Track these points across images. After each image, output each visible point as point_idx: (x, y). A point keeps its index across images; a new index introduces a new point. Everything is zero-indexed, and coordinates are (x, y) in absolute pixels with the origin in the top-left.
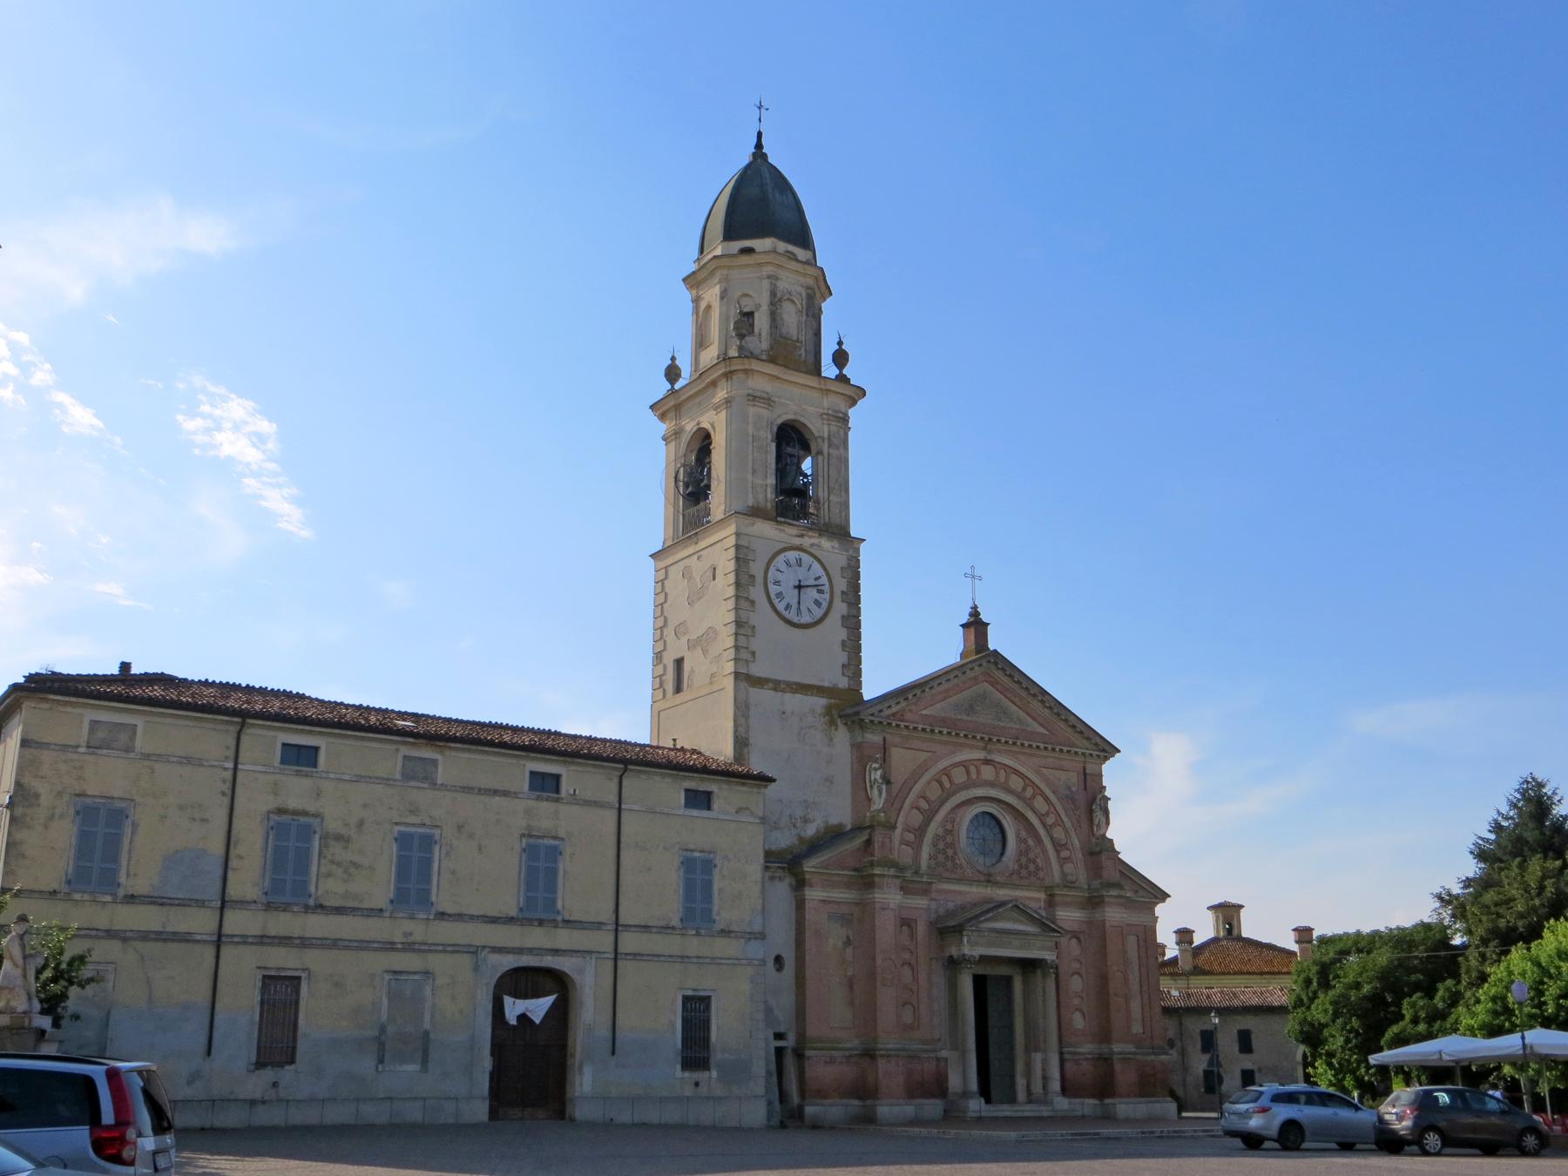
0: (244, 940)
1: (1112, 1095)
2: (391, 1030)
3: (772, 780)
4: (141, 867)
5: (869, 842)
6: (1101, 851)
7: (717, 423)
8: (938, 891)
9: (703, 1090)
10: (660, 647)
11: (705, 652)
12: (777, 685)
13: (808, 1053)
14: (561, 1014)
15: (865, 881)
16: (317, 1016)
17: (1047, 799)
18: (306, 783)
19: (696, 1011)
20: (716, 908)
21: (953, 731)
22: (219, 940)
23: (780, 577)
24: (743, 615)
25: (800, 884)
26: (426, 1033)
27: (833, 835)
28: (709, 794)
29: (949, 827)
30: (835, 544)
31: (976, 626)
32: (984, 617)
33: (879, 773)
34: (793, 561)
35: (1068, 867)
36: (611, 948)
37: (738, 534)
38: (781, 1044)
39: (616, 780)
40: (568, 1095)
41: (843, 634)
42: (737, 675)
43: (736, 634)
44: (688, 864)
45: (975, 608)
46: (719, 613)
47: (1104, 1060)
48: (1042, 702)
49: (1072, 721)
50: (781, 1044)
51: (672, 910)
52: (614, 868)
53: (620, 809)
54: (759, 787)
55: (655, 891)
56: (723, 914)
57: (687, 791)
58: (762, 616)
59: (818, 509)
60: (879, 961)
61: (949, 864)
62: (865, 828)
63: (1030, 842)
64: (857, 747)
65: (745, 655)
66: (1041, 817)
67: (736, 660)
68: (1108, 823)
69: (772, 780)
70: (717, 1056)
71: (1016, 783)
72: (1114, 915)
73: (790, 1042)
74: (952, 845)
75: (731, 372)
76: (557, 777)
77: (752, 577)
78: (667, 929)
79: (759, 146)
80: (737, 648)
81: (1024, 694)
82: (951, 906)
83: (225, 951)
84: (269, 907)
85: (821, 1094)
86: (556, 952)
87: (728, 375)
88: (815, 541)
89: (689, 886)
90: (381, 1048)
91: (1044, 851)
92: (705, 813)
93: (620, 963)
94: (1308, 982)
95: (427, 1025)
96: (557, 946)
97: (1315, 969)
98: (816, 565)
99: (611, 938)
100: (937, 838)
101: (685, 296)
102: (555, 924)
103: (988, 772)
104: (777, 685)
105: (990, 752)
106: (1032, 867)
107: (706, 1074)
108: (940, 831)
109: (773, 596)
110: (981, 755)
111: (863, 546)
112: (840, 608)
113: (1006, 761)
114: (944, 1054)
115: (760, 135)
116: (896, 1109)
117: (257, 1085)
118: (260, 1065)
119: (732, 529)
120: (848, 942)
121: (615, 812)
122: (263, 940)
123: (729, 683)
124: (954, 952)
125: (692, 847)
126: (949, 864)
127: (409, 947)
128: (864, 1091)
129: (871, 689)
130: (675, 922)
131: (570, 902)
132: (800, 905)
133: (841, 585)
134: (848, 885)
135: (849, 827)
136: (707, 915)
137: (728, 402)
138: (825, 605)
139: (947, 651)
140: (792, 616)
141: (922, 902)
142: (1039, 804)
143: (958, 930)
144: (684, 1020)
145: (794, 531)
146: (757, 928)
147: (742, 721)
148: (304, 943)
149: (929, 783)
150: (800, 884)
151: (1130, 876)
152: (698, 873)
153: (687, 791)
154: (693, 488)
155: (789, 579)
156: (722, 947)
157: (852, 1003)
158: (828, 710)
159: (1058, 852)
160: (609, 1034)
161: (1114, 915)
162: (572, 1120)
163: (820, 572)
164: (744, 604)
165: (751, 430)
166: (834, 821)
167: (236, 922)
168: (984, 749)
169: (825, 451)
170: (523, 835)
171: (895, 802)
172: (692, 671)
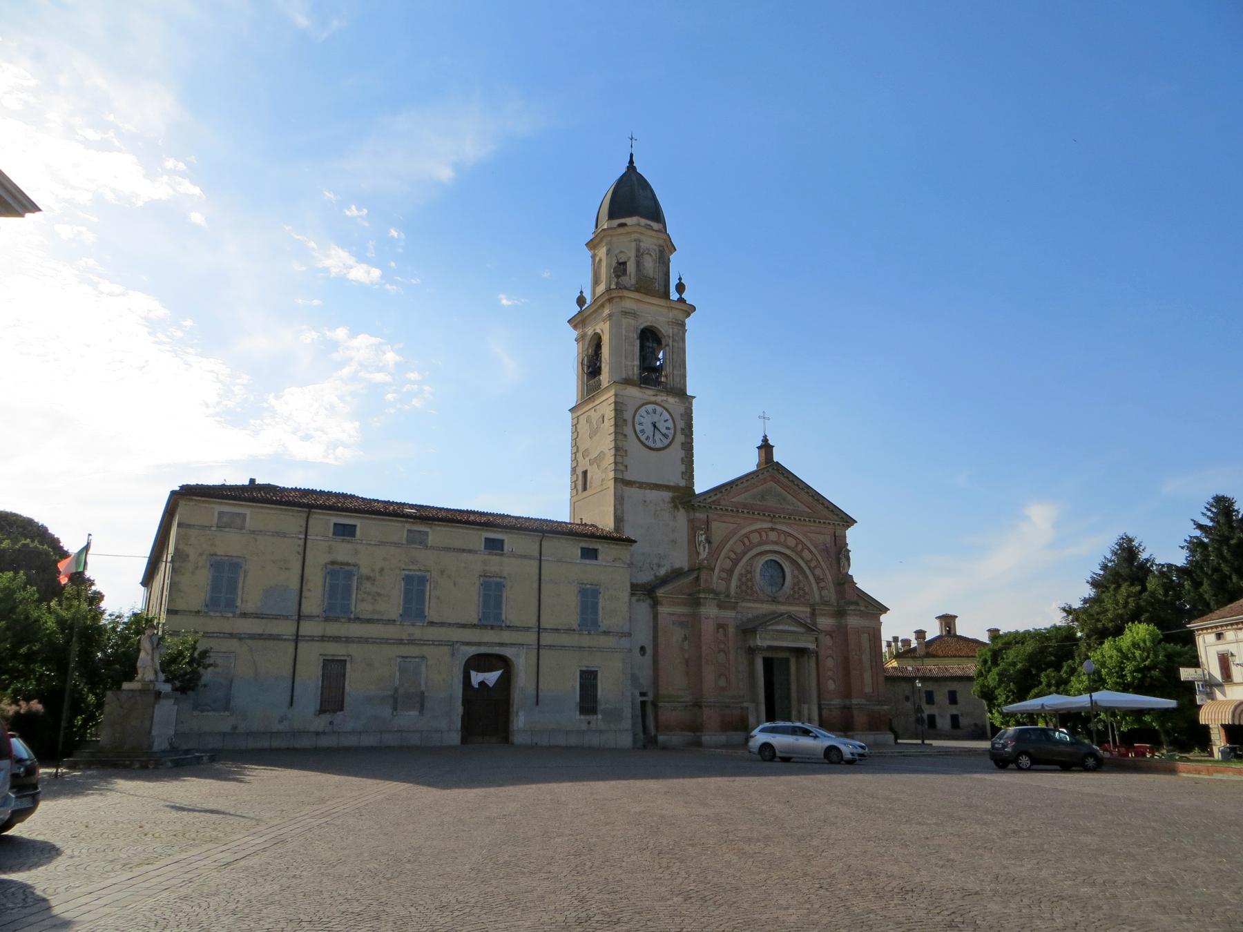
0: (312, 639)
2: (401, 691)
3: (635, 542)
4: (250, 596)
6: (845, 582)
7: (603, 328)
12: (641, 485)
15: (695, 602)
16: (356, 684)
17: (811, 552)
18: (349, 546)
19: (589, 680)
21: (752, 511)
22: (297, 639)
23: (642, 420)
25: (655, 603)
26: (423, 693)
27: (677, 574)
31: (766, 448)
32: (771, 442)
35: (824, 593)
37: (616, 395)
38: (644, 699)
41: (682, 454)
42: (616, 479)
45: (765, 437)
47: (847, 709)
50: (644, 699)
51: (573, 620)
55: (563, 608)
56: (605, 622)
58: (632, 445)
60: (704, 648)
62: (696, 570)
63: (801, 577)
65: (621, 467)
70: (601, 706)
72: (853, 621)
73: (649, 698)
74: (751, 580)
76: (502, 541)
77: (625, 421)
78: (570, 631)
79: (631, 162)
80: (616, 463)
83: (300, 645)
84: (327, 619)
87: (610, 300)
90: (396, 701)
92: (594, 562)
94: (985, 662)
95: (423, 688)
98: (665, 413)
99: (535, 636)
102: (501, 628)
103: (773, 536)
110: (769, 525)
113: (784, 528)
115: (631, 155)
117: (320, 723)
118: (322, 711)
119: (612, 392)
120: (685, 638)
121: (536, 563)
122: (323, 638)
123: (611, 484)
124: (752, 644)
127: (412, 642)
128: (696, 727)
129: (700, 487)
130: (575, 627)
132: (655, 617)
133: (681, 424)
136: (595, 623)
137: (610, 316)
139: (749, 462)
141: (731, 614)
142: (806, 554)
145: (651, 392)
146: (626, 629)
148: (348, 640)
154: (592, 368)
156: (604, 641)
158: (673, 500)
161: (853, 621)
166: (677, 566)
167: (308, 628)
171: (714, 554)
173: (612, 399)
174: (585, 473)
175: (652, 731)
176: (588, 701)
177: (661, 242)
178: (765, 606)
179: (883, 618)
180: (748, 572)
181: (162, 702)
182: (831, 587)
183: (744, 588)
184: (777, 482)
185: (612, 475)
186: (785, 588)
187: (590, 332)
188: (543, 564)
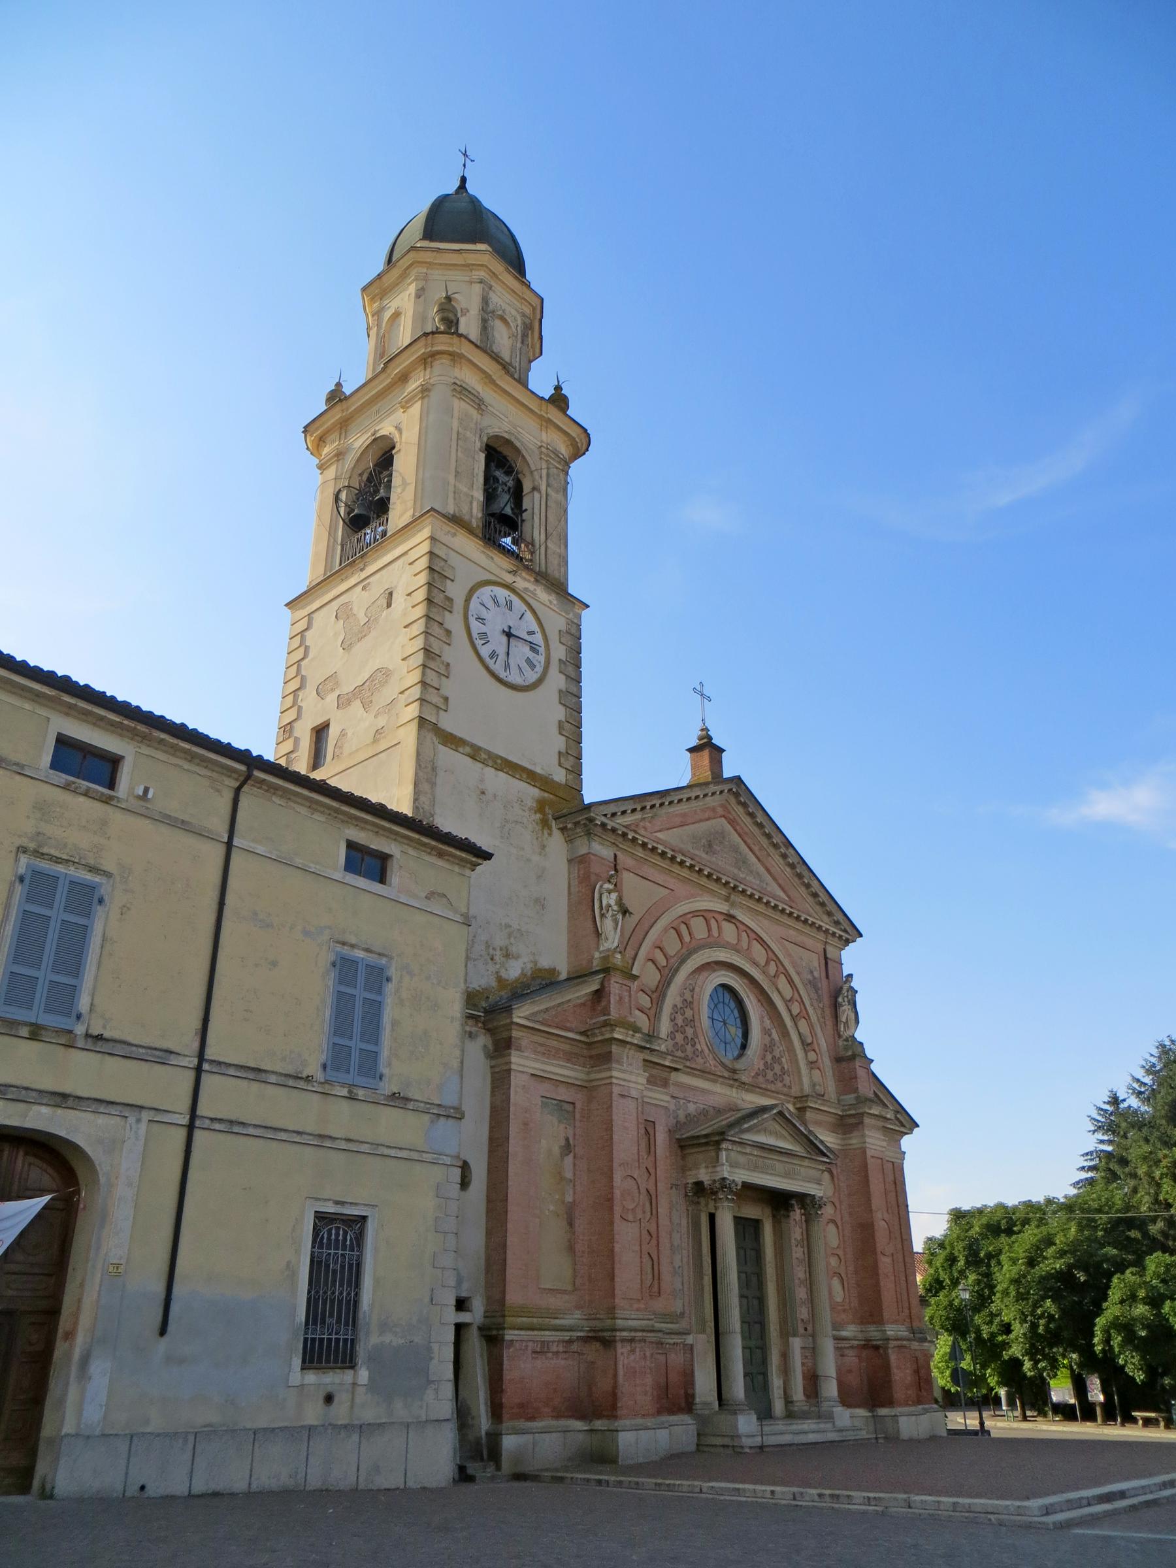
1: (890, 1403)
3: (487, 856)
5: (599, 994)
6: (850, 1058)
7: (404, 425)
8: (679, 1085)
9: (340, 1412)
10: (291, 715)
11: (366, 706)
12: (476, 753)
13: (509, 1335)
14: (53, 1243)
15: (596, 1052)
17: (791, 981)
19: (338, 1243)
20: (385, 1053)
23: (484, 613)
24: (436, 647)
25: (501, 1046)
27: (543, 982)
28: (384, 858)
29: (688, 996)
30: (553, 598)
31: (707, 748)
33: (614, 896)
34: (502, 601)
36: (184, 1105)
37: (433, 539)
38: (465, 1317)
39: (228, 796)
40: (47, 1431)
41: (560, 713)
42: (422, 721)
43: (424, 666)
44: (345, 968)
45: (706, 729)
46: (396, 648)
48: (784, 856)
49: (815, 887)
50: (465, 1317)
52: (212, 918)
53: (229, 845)
54: (462, 862)
55: (279, 1010)
56: (397, 1070)
57: (351, 845)
58: (458, 654)
59: (532, 553)
61: (689, 1047)
62: (597, 977)
63: (775, 1035)
64: (579, 862)
65: (434, 698)
66: (788, 1002)
67: (422, 700)
68: (857, 1022)
69: (487, 856)
70: (370, 1340)
71: (758, 952)
72: (874, 1141)
73: (475, 1315)
74: (691, 1022)
75: (433, 355)
76: (114, 761)
77: (450, 600)
78: (295, 1080)
80: (424, 683)
81: (764, 842)
82: (692, 1108)
85: (528, 1412)
86: (62, 1099)
87: (427, 360)
88: (531, 587)
89: (343, 1007)
91: (791, 1049)
92: (376, 887)
93: (198, 1135)
94: (952, 1260)
96: (67, 1088)
97: (959, 1246)
98: (529, 615)
100: (676, 1010)
101: (283, 623)
104: (476, 753)
105: (733, 905)
106: (777, 1068)
107: (348, 1376)
108: (678, 1001)
109: (475, 635)
110: (723, 907)
111: (586, 615)
112: (556, 680)
114: (690, 1339)
116: (645, 1435)
119: (426, 532)
120: (567, 1148)
121: (221, 850)
123: (408, 736)
124: (704, 1175)
125: (353, 940)
126: (689, 1047)
128: (595, 1404)
130: (313, 1068)
131: (104, 999)
132: (500, 1080)
133: (559, 652)
134: (570, 1057)
135: (563, 976)
136: (370, 1066)
137: (425, 390)
138: (539, 669)
140: (498, 668)
142: (782, 982)
143: (714, 1141)
144: (315, 1263)
146: (450, 1100)
147: (426, 787)
149: (666, 930)
150: (501, 1046)
151: (882, 1095)
152: (359, 988)
153: (351, 845)
154: (364, 510)
155: (496, 622)
157: (571, 1249)
158: (541, 806)
159: (806, 1052)
160: (159, 1288)
161: (874, 1141)
162: (47, 1494)
163: (534, 627)
164: (436, 630)
165: (455, 424)
166: (545, 963)
168: (727, 899)
169: (543, 488)
170: (22, 850)
172: (343, 734)
173: (425, 547)
174: (320, 732)
175: (484, 1423)
176: (331, 1332)
177: (528, 311)
178: (718, 1088)
179: (906, 1142)
180: (688, 1004)
181: (687, 1418)
182: (826, 1062)
183: (679, 1037)
184: (732, 822)
185: (413, 711)
186: (749, 1052)
187: (359, 441)
188: (236, 859)
